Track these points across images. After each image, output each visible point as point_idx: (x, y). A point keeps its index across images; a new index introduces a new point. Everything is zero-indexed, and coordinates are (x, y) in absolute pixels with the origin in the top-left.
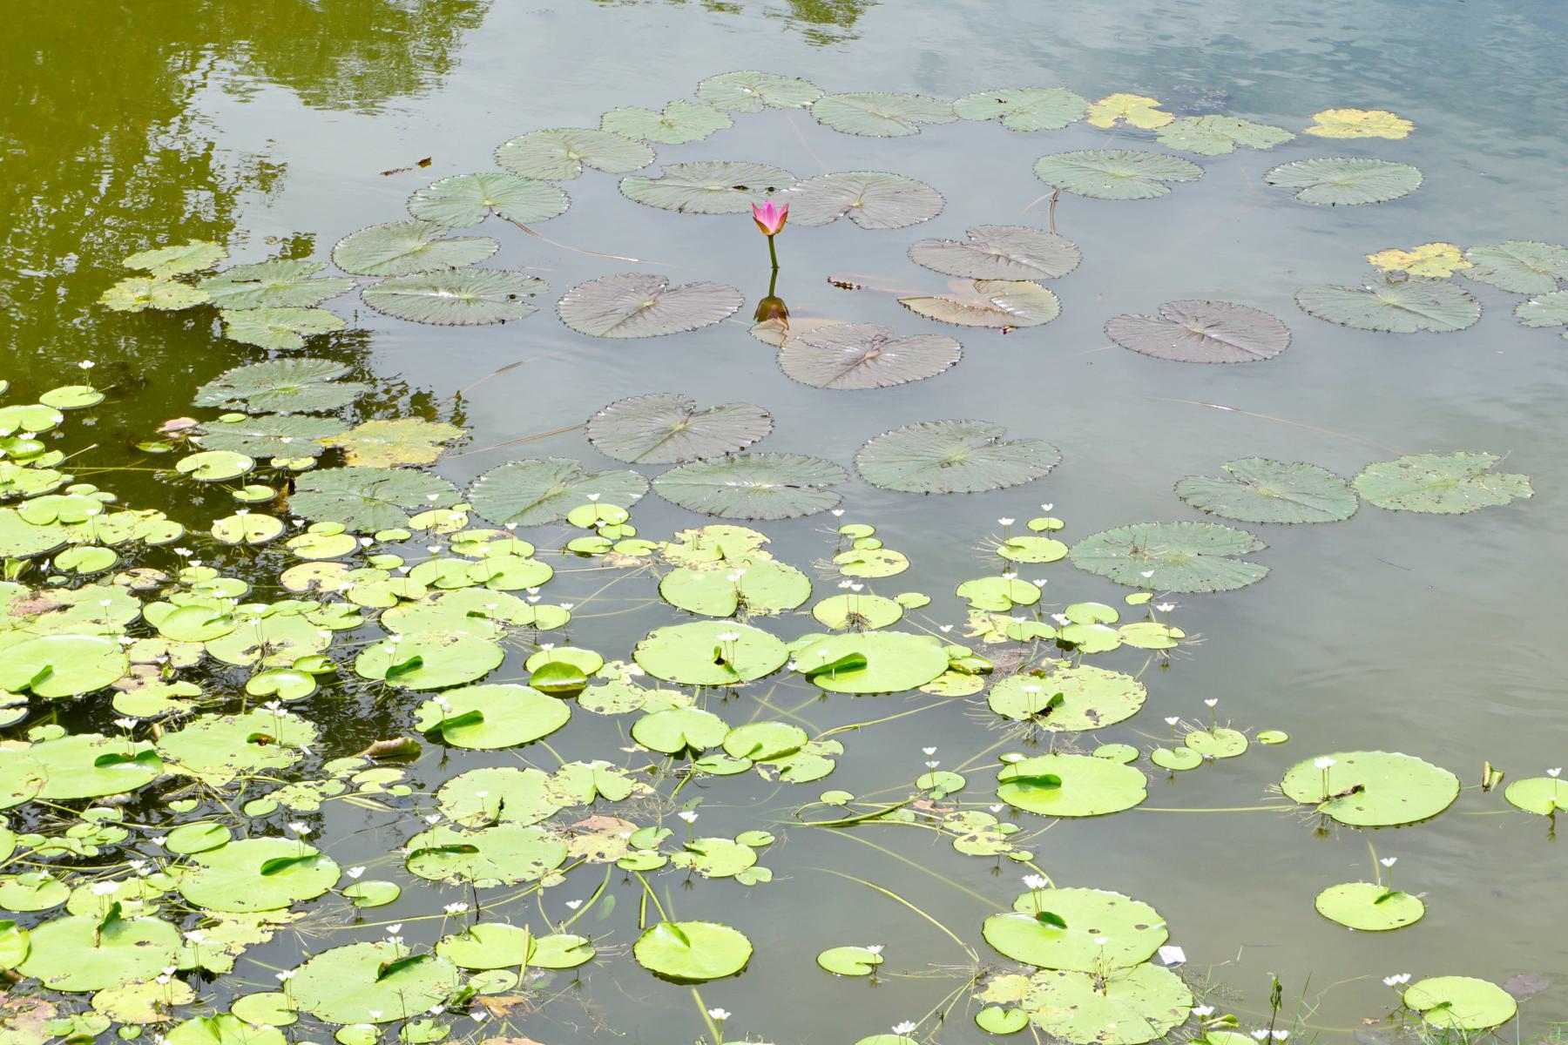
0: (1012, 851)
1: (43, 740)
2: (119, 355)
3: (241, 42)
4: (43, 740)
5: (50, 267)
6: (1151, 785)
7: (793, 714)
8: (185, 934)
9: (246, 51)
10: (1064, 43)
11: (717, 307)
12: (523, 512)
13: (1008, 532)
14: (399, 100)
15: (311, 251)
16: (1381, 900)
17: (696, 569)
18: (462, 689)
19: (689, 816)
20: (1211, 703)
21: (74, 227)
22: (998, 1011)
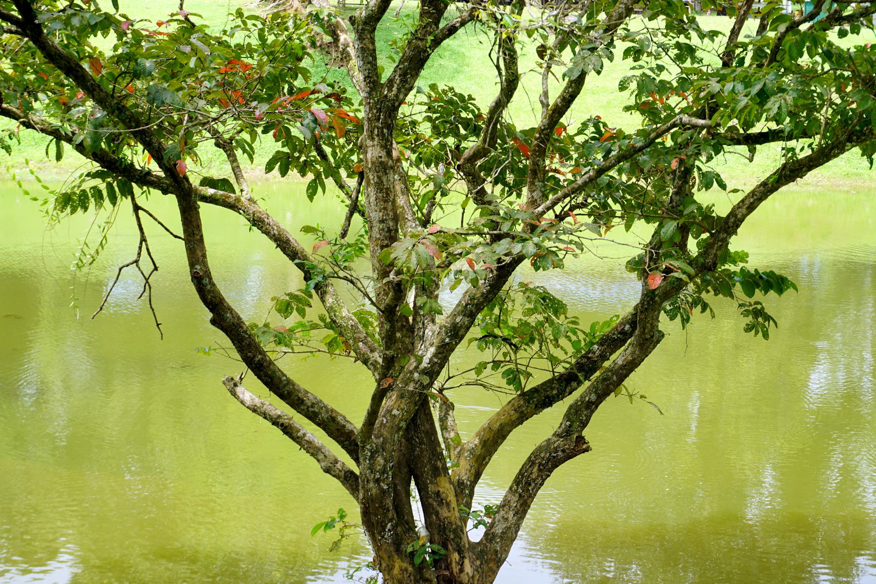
1: (776, 326)
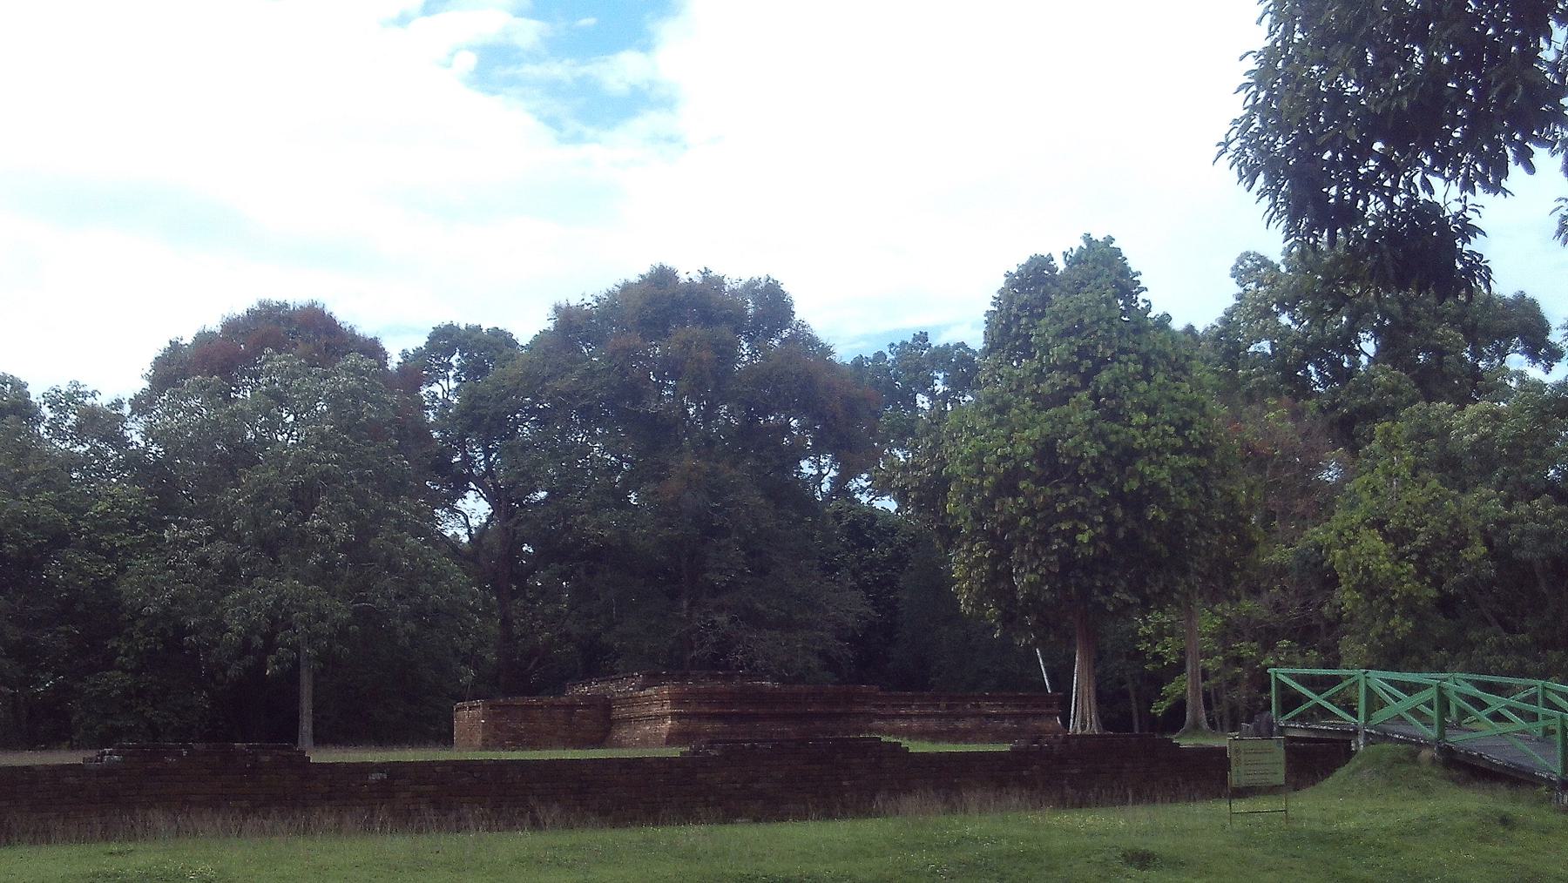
0: (821, 492)
1: (1241, 59)
2: (950, 539)
3: (674, 752)
4: (1241, 59)
5: (1032, 771)
6: (433, 764)
7: (1328, 699)
8: (1429, 177)
9: (1209, 667)
10: (1100, 852)
11: (1086, 701)
12: (1559, 208)
13: (1124, 609)
14: (1312, 787)
15: (1233, 276)
16: (1485, 235)
17: (1415, 612)
18: (1243, 53)
19: (1518, 137)
20: (1485, 147)
21: (1429, 59)
22: (1564, 200)
